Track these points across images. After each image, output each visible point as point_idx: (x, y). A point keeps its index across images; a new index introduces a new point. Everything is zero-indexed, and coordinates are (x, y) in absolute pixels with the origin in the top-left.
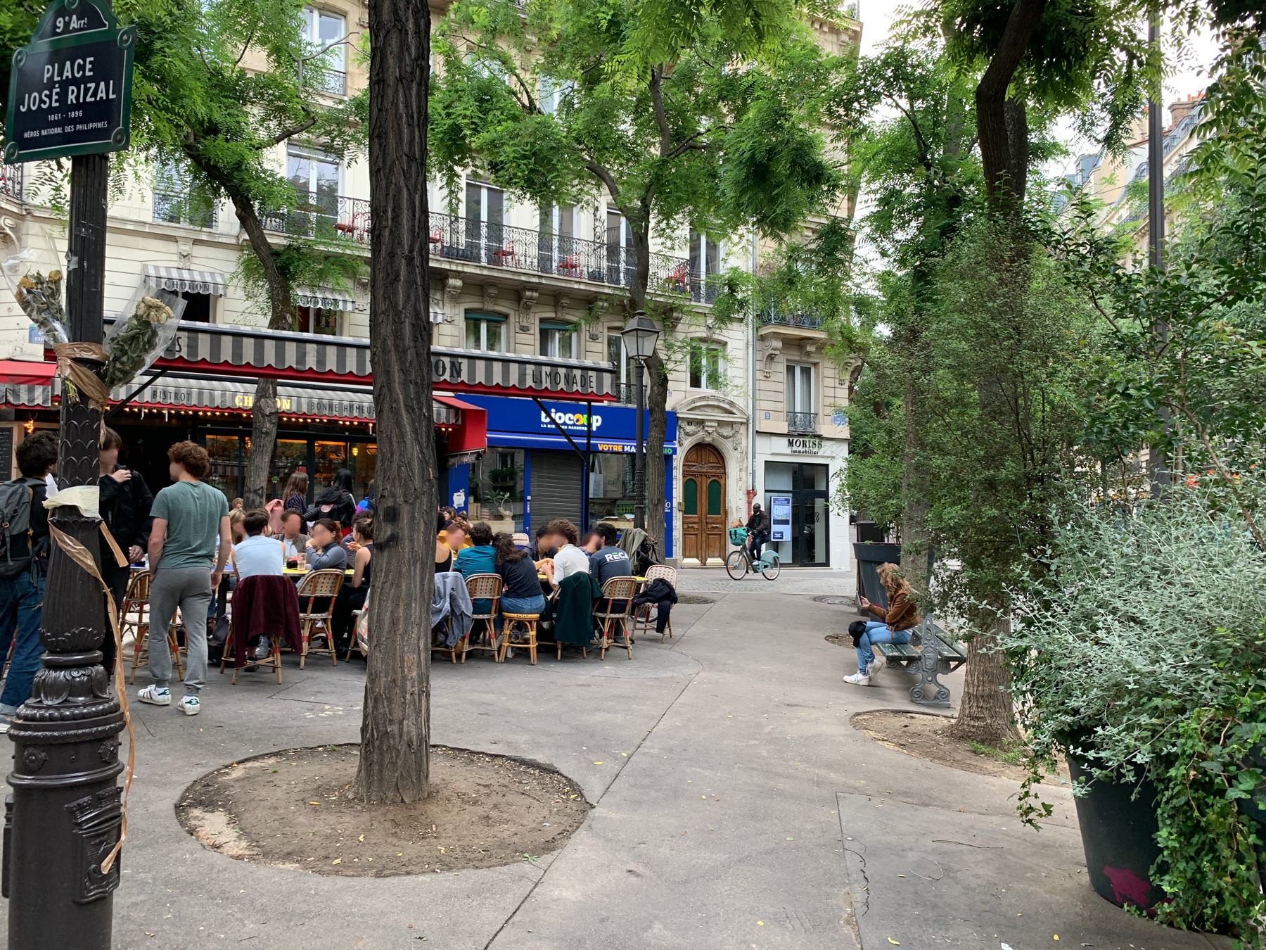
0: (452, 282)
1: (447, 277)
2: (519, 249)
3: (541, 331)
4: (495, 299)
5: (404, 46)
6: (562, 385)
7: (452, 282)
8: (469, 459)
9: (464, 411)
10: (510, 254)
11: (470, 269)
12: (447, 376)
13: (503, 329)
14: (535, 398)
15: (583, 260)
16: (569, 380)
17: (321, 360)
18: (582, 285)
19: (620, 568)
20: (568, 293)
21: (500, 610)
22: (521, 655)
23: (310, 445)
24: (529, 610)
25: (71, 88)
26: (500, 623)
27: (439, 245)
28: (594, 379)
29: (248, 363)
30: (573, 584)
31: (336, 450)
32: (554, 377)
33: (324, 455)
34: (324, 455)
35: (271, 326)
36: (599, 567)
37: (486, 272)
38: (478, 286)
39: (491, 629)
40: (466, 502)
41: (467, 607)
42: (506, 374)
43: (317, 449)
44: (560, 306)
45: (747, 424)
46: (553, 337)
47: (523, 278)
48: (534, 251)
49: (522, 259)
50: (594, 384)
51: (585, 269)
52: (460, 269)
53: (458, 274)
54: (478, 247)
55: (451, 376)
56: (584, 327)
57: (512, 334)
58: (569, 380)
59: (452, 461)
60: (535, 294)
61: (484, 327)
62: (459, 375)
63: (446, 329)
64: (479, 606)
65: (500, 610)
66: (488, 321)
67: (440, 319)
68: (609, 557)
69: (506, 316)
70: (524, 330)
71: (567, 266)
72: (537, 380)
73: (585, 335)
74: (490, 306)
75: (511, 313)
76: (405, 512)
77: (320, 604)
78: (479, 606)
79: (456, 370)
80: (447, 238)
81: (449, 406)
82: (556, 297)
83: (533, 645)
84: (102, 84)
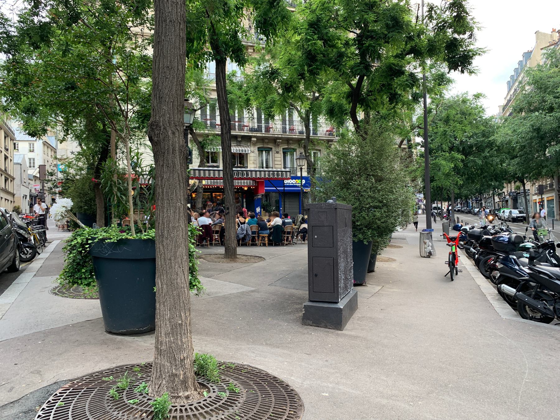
0: (253, 139)
3: (283, 152)
5: (226, 127)
6: (276, 176)
7: (253, 139)
8: (260, 197)
11: (259, 135)
12: (245, 176)
13: (271, 152)
16: (278, 175)
17: (214, 175)
18: (296, 136)
19: (289, 223)
20: (292, 139)
21: (258, 234)
22: (264, 245)
23: (212, 195)
24: (265, 234)
26: (258, 237)
30: (276, 227)
31: (219, 196)
32: (273, 174)
33: (215, 197)
34: (215, 197)
36: (284, 223)
38: (261, 140)
39: (257, 238)
40: (261, 211)
41: (250, 233)
42: (260, 174)
43: (214, 196)
44: (288, 144)
53: (255, 137)
58: (278, 175)
59: (255, 197)
63: (252, 154)
64: (253, 233)
65: (258, 234)
66: (266, 151)
67: (249, 152)
68: (286, 221)
69: (271, 149)
70: (277, 152)
71: (292, 130)
72: (269, 175)
74: (266, 146)
75: (273, 147)
76: (230, 208)
77: (217, 232)
78: (253, 233)
79: (247, 175)
80: (251, 125)
82: (288, 141)
83: (266, 242)
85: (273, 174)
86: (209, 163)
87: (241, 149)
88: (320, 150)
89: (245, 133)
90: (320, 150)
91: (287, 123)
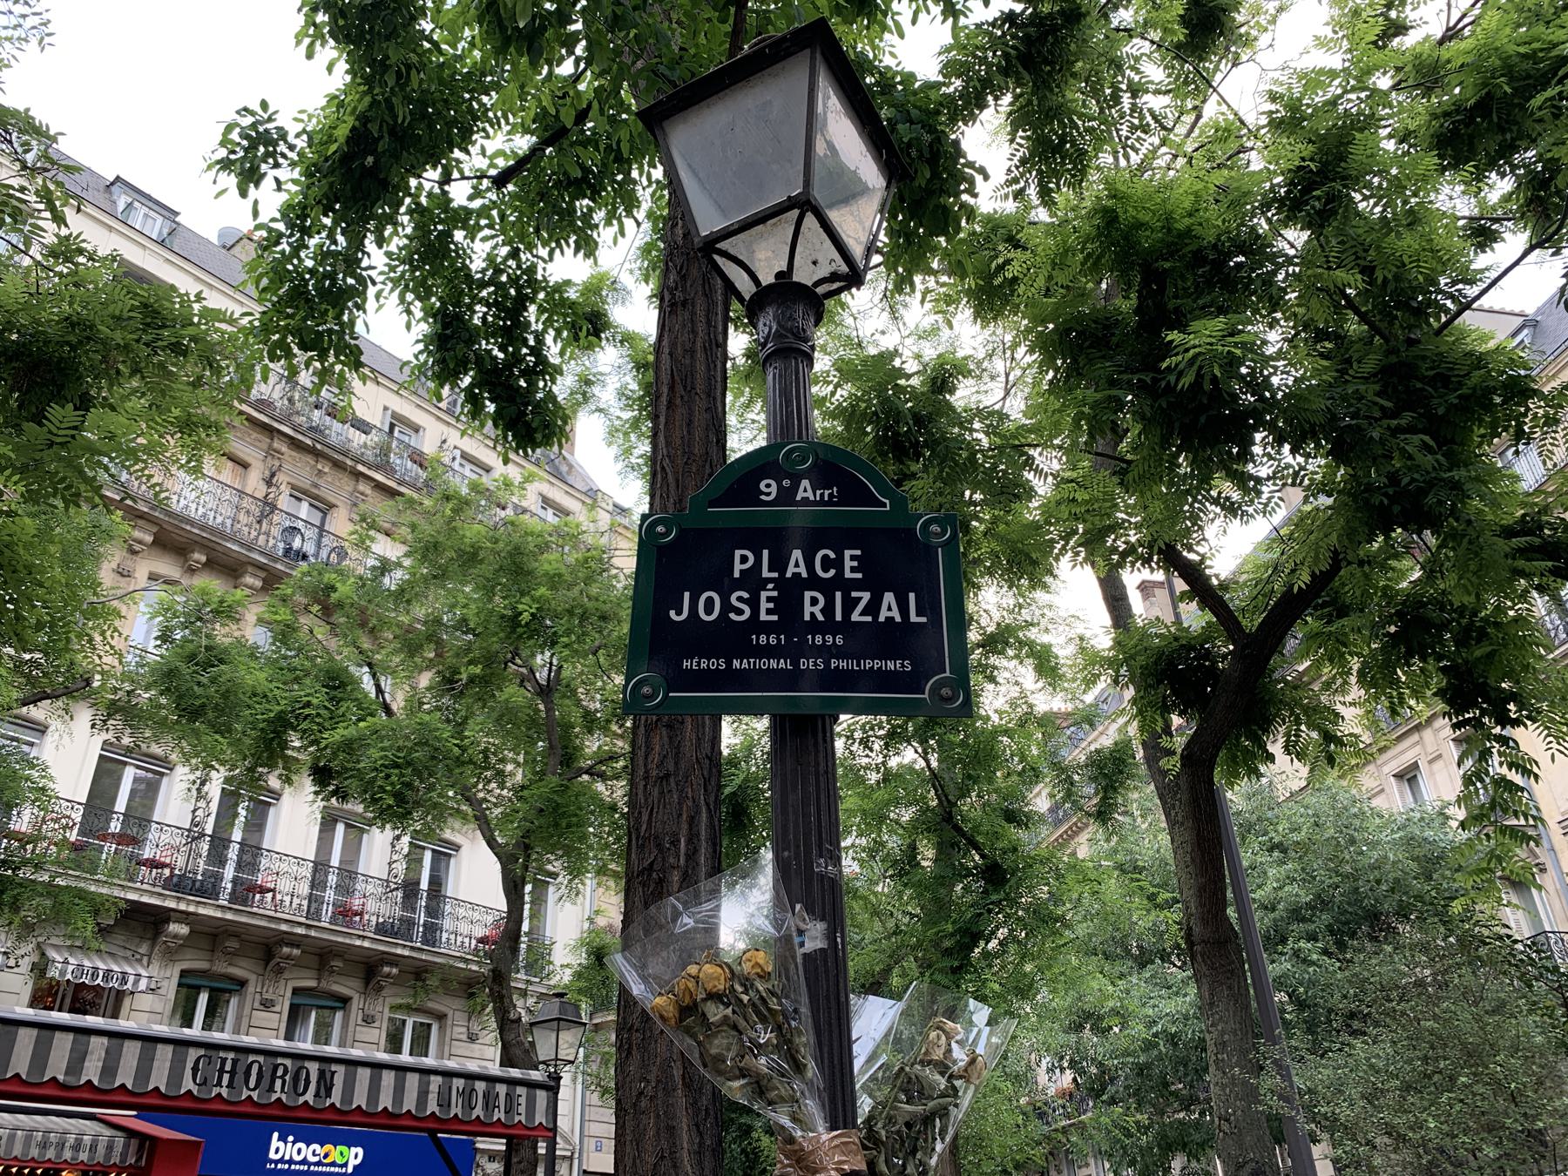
1: (167, 921)
2: (284, 885)
4: (232, 955)
6: (478, 1111)
9: (154, 1140)
10: (269, 890)
14: (432, 1133)
15: (371, 906)
16: (490, 1101)
25: (808, 595)
27: (167, 872)
28: (523, 1100)
29: (123, 1086)
32: (468, 1096)
35: (35, 1002)
37: (229, 916)
38: (211, 936)
45: (571, 1158)
46: (306, 1018)
47: (284, 927)
48: (304, 889)
49: (287, 899)
50: (522, 1109)
51: (374, 919)
52: (192, 909)
53: (185, 917)
54: (218, 878)
55: (317, 1095)
56: (357, 1003)
57: (247, 1011)
60: (296, 952)
61: (203, 999)
62: (329, 1095)
67: (143, 985)
69: (242, 983)
70: (267, 1005)
71: (345, 913)
72: (444, 1103)
73: (355, 1013)
74: (222, 967)
75: (252, 978)
81: (130, 1133)
82: (324, 956)
84: (889, 597)
85: (468, 1096)
86: (188, 1022)
87: (101, 965)
88: (441, 1017)
89: (144, 892)
90: (441, 1017)
91: (233, 853)
